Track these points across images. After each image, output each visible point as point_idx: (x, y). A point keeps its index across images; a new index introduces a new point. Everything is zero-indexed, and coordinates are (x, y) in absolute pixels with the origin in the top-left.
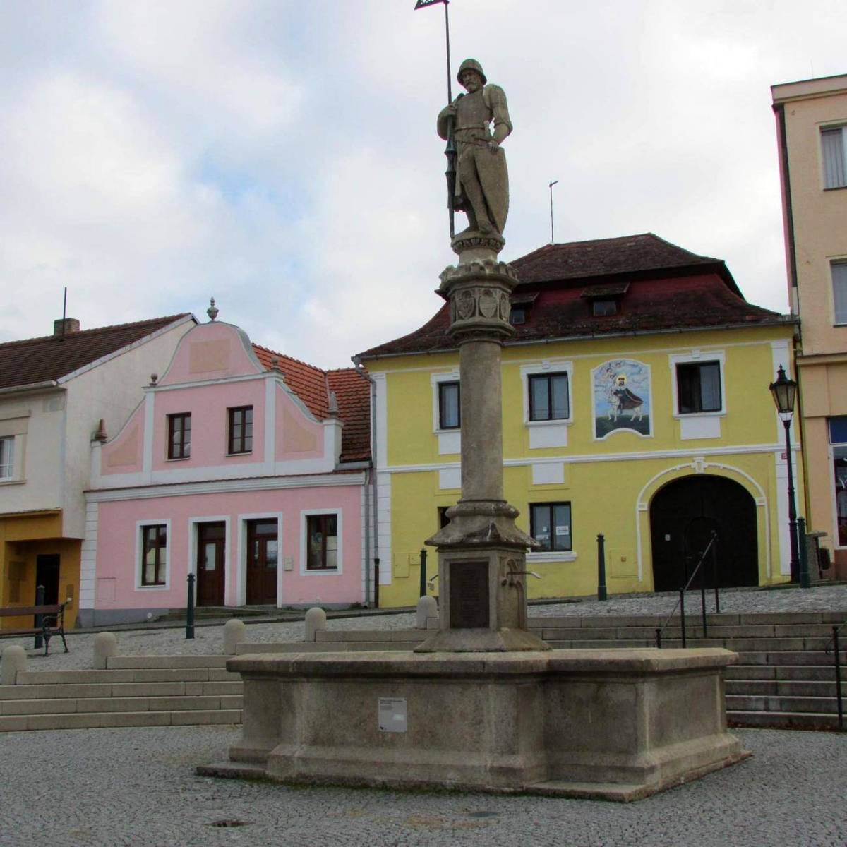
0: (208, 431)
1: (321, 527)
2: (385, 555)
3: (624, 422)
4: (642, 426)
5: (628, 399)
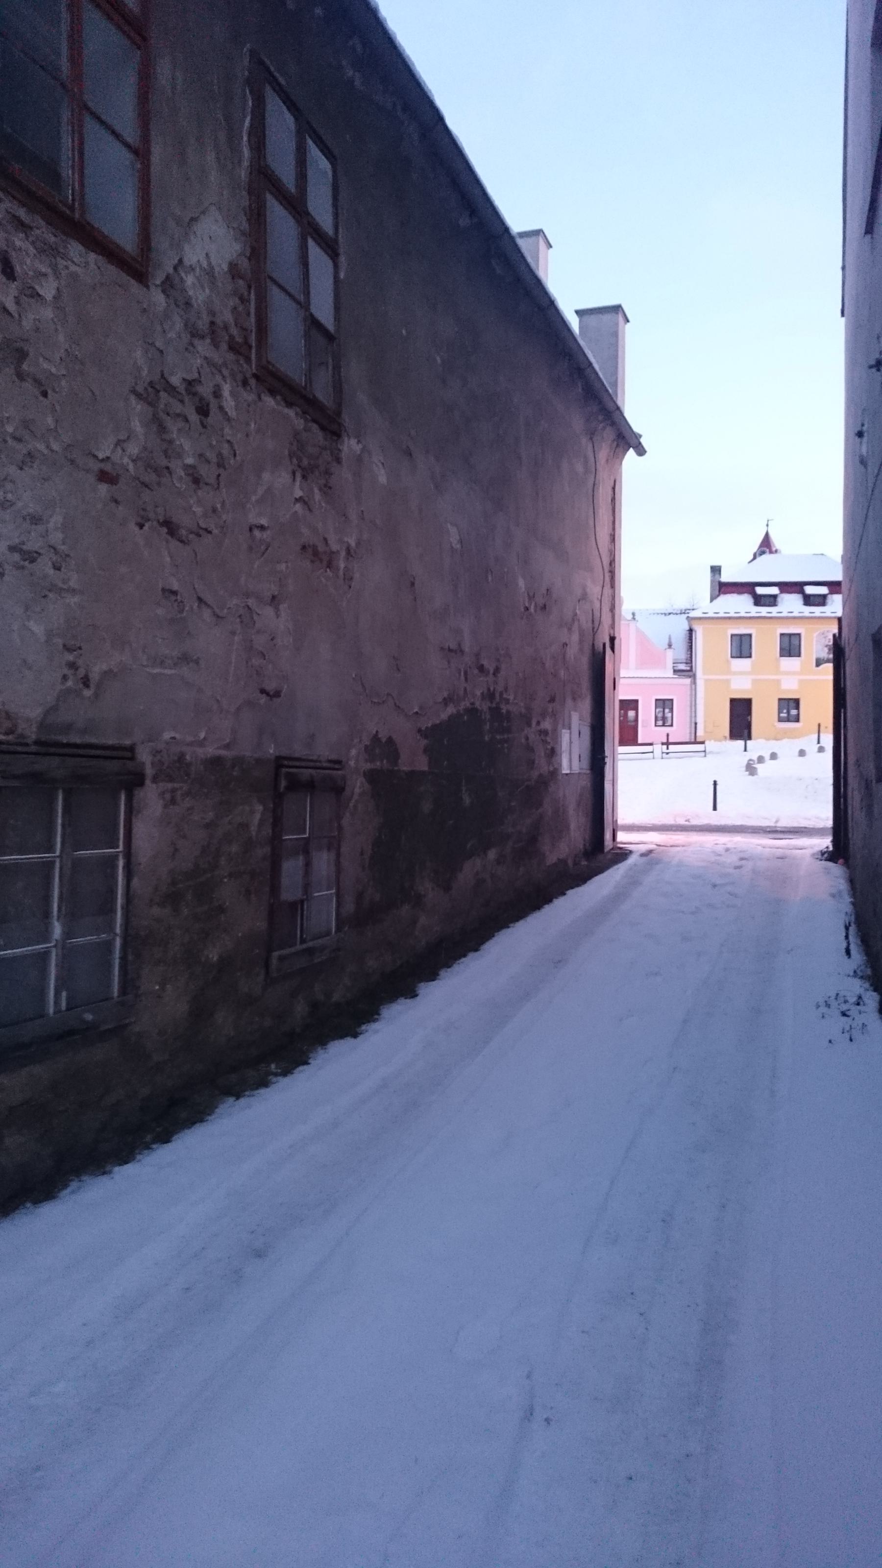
1: (664, 704)
2: (700, 720)
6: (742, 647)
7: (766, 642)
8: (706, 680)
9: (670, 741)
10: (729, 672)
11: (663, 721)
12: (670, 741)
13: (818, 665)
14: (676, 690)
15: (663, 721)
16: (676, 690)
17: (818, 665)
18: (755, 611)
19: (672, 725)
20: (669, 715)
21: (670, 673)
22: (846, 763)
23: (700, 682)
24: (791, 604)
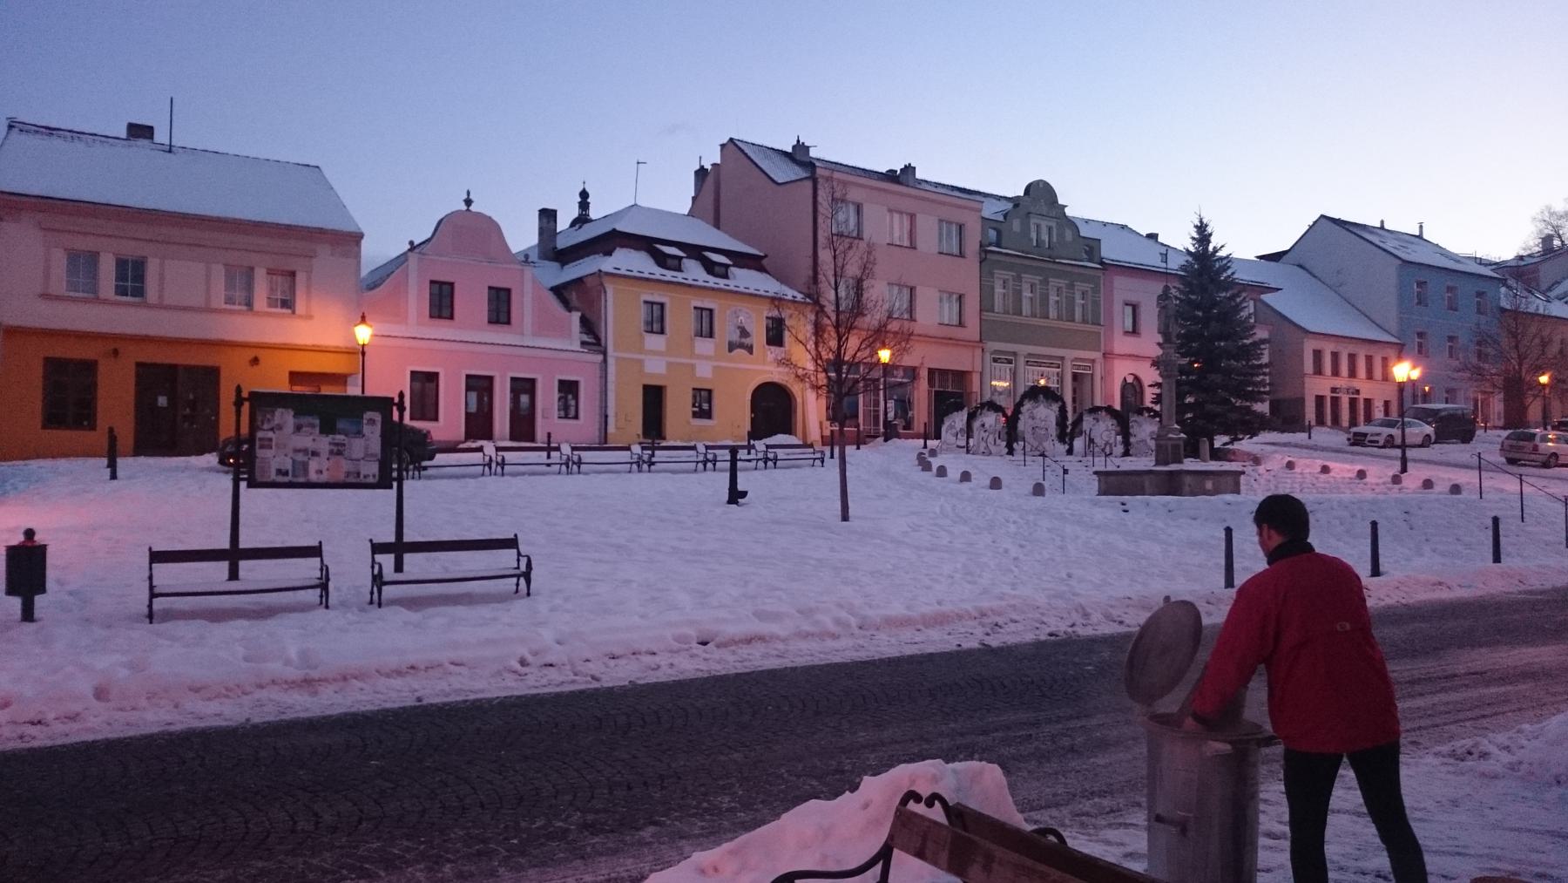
0: (471, 303)
1: (569, 389)
2: (611, 412)
3: (741, 346)
4: (750, 349)
5: (744, 333)
6: (656, 322)
7: (680, 317)
8: (617, 359)
9: (409, 537)
10: (642, 350)
11: (568, 410)
12: (409, 537)
13: (730, 350)
14: (582, 368)
15: (568, 410)
16: (582, 368)
17: (730, 350)
18: (659, 272)
19: (576, 417)
20: (573, 403)
21: (577, 347)
22: (902, 195)
23: (611, 361)
24: (694, 272)
